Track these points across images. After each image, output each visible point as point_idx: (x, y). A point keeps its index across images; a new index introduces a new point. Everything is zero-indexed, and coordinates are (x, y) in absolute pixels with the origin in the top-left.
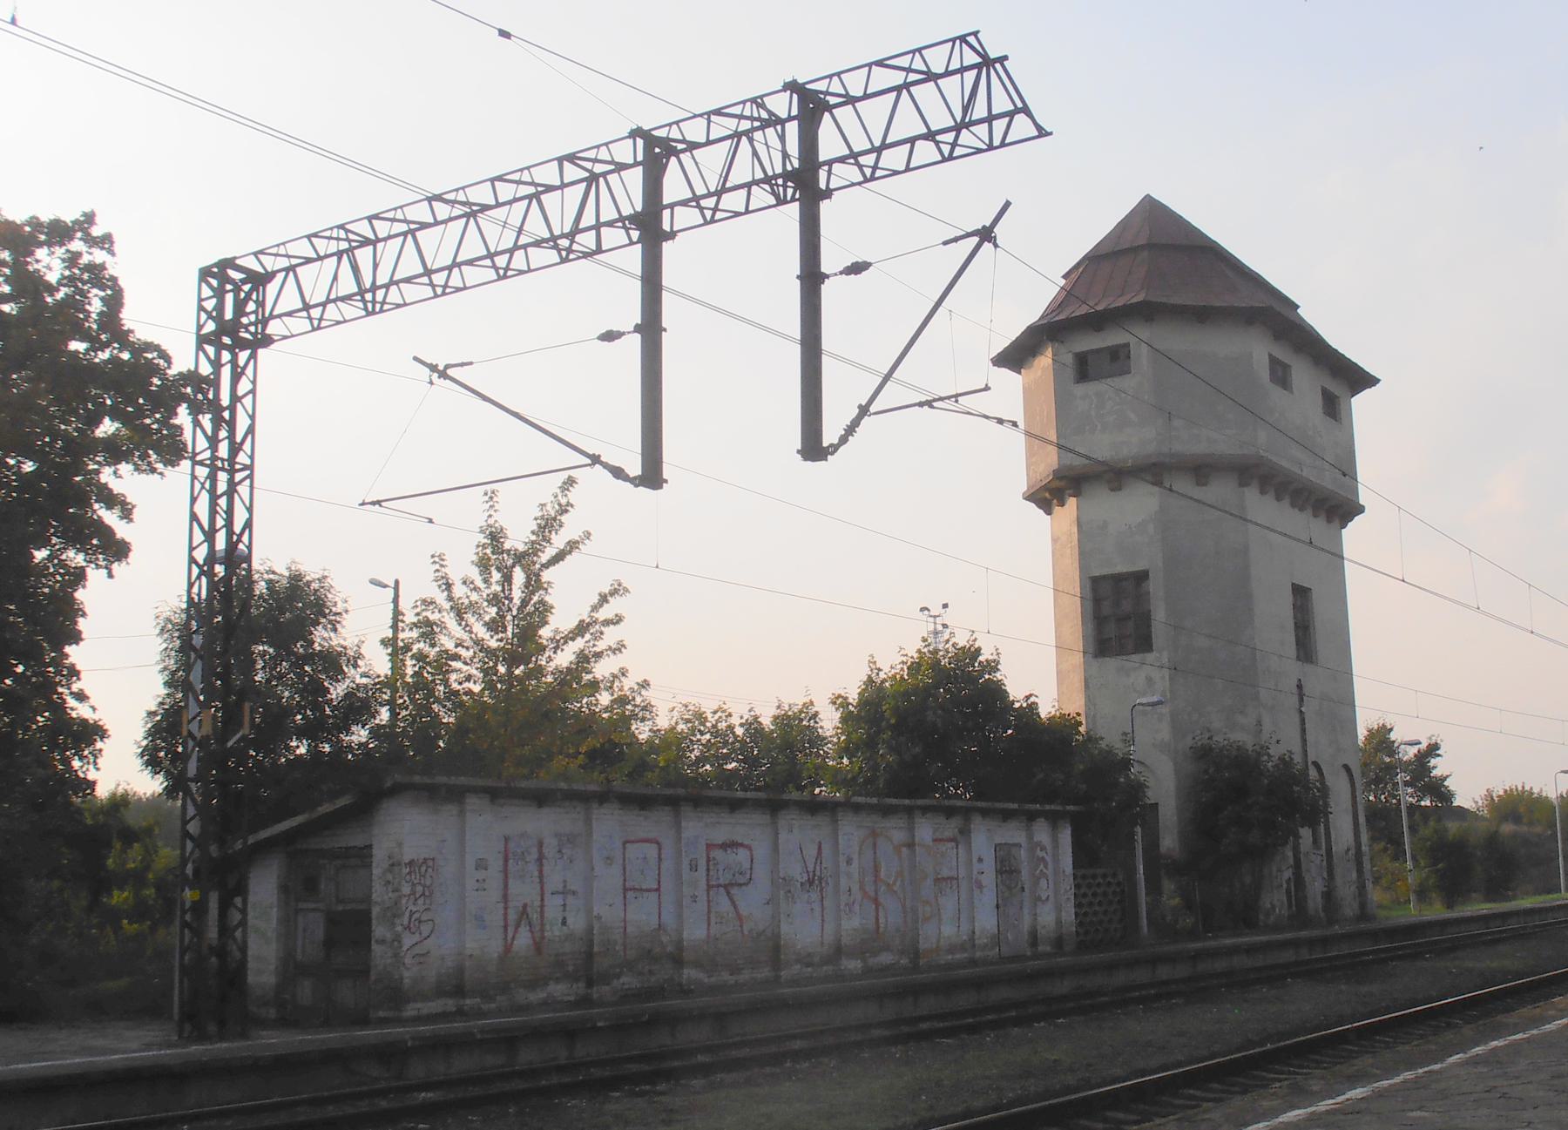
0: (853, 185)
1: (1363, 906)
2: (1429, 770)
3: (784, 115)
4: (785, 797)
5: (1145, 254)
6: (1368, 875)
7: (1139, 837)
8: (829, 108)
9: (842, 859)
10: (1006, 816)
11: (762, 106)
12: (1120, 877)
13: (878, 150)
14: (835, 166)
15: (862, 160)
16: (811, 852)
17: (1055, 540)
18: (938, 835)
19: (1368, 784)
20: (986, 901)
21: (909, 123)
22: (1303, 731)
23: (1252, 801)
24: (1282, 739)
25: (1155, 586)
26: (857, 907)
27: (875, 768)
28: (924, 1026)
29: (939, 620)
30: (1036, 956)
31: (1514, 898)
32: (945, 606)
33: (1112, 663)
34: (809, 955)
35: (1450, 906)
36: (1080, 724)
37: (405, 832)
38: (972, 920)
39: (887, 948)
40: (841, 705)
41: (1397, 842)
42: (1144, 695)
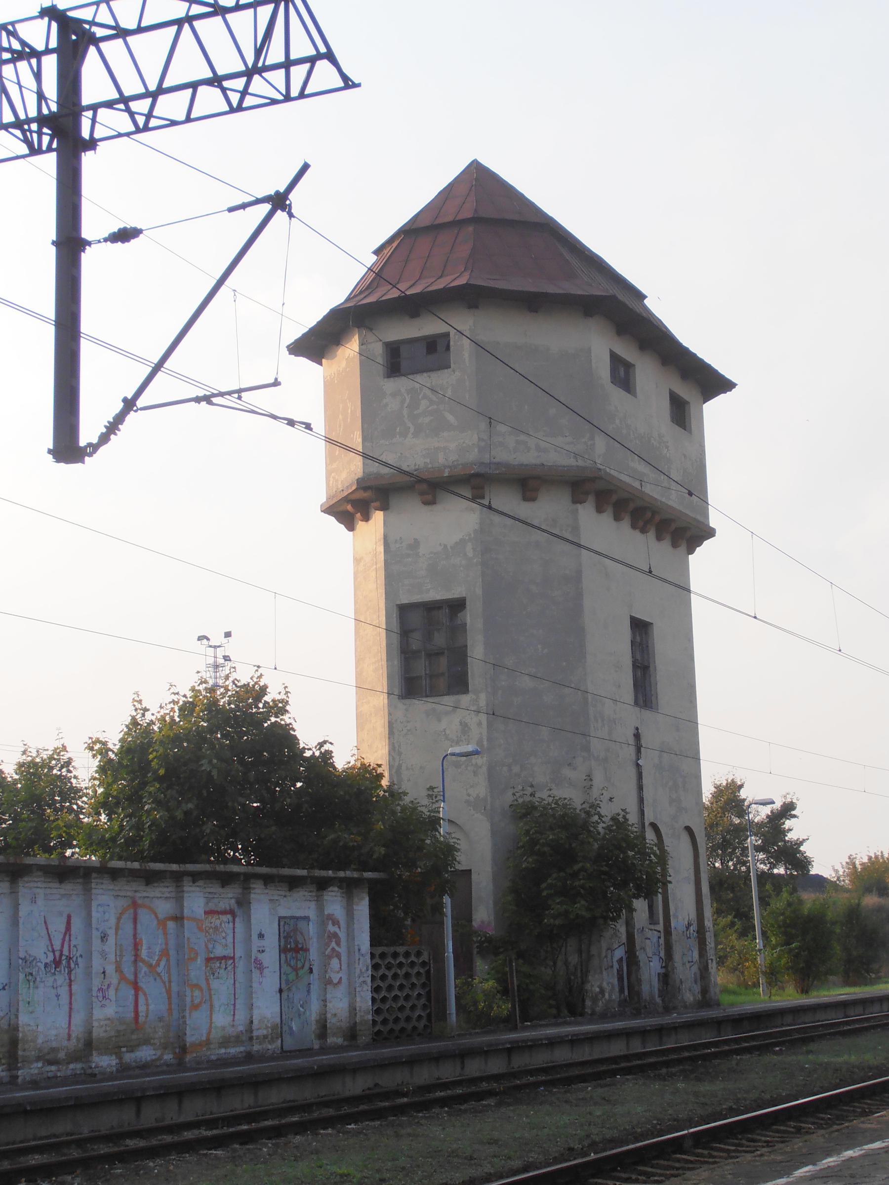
0: (120, 135)
1: (705, 991)
2: (784, 833)
3: (40, 47)
4: (29, 861)
5: (471, 229)
6: (711, 954)
7: (448, 911)
8: (95, 41)
9: (96, 935)
10: (293, 883)
11: (13, 34)
12: (425, 957)
13: (154, 95)
14: (102, 112)
15: (134, 106)
16: (58, 926)
17: (357, 560)
18: (212, 906)
19: (714, 849)
20: (268, 983)
21: (189, 66)
22: (640, 788)
23: (581, 869)
24: (615, 798)
25: (473, 619)
26: (111, 993)
27: (139, 827)
28: (188, 1135)
29: (220, 653)
30: (323, 1050)
31: (872, 982)
32: (228, 635)
33: (420, 706)
34: (54, 1050)
35: (805, 991)
36: (380, 776)
38: (251, 1007)
39: (147, 1042)
40: (100, 752)
41: (744, 915)
42: (458, 743)
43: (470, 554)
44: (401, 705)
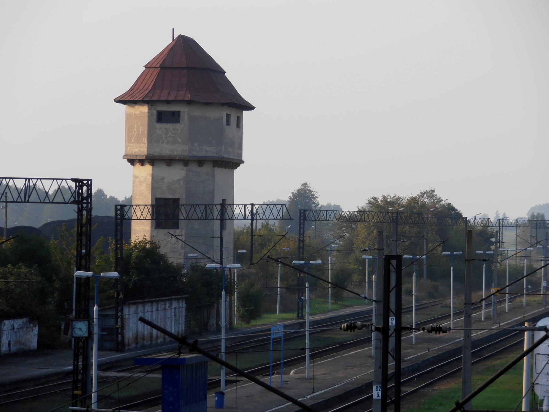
5: (185, 71)
37: (86, 323)
43: (182, 184)
44: (155, 231)
